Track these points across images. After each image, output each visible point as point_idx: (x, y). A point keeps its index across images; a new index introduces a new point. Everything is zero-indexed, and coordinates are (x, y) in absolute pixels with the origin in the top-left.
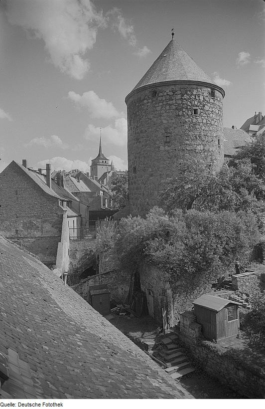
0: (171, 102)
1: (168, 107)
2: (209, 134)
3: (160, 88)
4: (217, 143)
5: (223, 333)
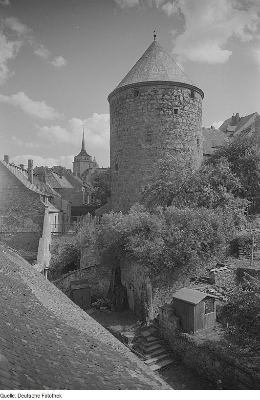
0: (152, 102)
2: (188, 134)
3: (142, 88)
4: (196, 142)
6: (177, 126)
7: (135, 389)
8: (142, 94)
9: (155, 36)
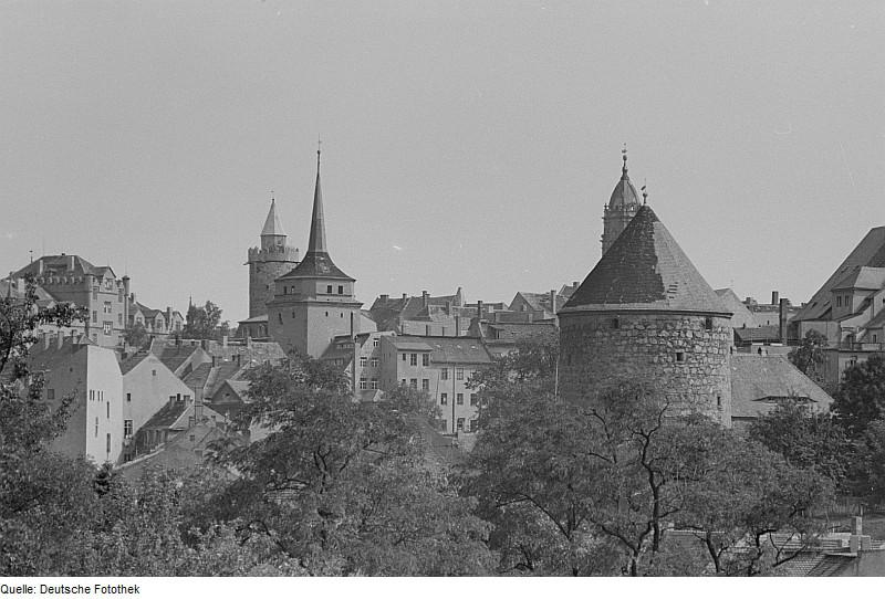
0: (641, 341)
1: (635, 349)
2: (701, 392)
3: (624, 317)
4: (715, 403)
5: (674, 288)
6: (682, 380)
7: (443, 575)
8: (625, 327)
9: (625, 159)
